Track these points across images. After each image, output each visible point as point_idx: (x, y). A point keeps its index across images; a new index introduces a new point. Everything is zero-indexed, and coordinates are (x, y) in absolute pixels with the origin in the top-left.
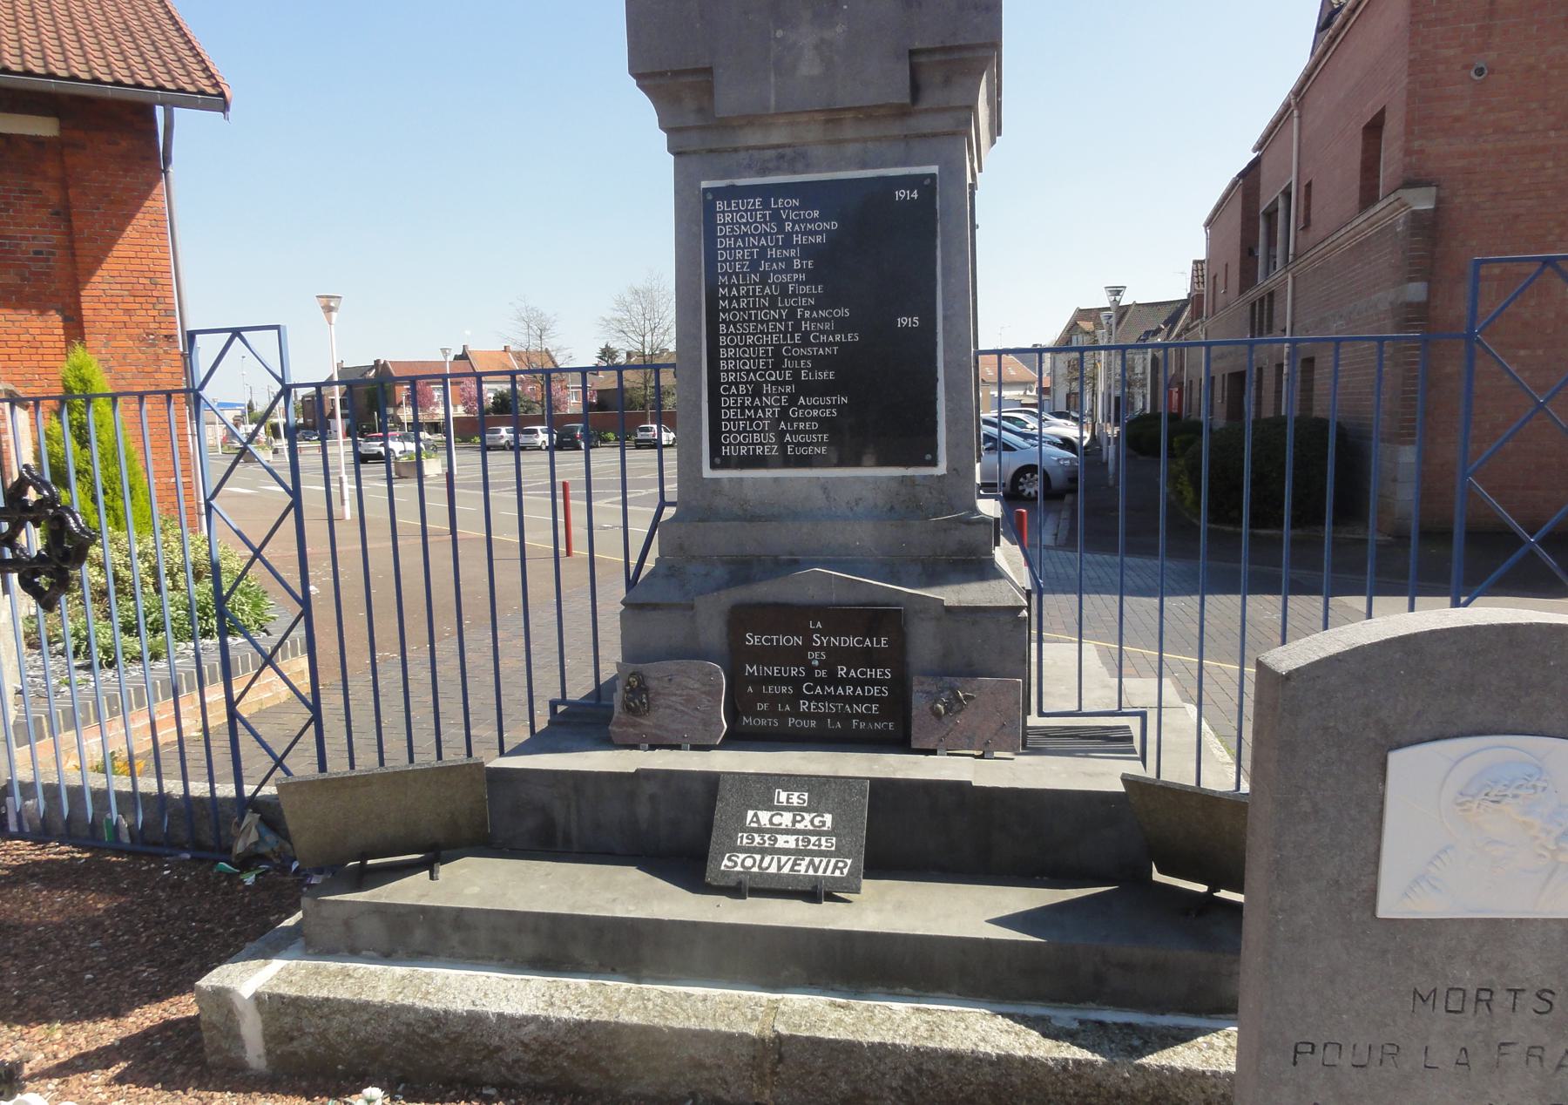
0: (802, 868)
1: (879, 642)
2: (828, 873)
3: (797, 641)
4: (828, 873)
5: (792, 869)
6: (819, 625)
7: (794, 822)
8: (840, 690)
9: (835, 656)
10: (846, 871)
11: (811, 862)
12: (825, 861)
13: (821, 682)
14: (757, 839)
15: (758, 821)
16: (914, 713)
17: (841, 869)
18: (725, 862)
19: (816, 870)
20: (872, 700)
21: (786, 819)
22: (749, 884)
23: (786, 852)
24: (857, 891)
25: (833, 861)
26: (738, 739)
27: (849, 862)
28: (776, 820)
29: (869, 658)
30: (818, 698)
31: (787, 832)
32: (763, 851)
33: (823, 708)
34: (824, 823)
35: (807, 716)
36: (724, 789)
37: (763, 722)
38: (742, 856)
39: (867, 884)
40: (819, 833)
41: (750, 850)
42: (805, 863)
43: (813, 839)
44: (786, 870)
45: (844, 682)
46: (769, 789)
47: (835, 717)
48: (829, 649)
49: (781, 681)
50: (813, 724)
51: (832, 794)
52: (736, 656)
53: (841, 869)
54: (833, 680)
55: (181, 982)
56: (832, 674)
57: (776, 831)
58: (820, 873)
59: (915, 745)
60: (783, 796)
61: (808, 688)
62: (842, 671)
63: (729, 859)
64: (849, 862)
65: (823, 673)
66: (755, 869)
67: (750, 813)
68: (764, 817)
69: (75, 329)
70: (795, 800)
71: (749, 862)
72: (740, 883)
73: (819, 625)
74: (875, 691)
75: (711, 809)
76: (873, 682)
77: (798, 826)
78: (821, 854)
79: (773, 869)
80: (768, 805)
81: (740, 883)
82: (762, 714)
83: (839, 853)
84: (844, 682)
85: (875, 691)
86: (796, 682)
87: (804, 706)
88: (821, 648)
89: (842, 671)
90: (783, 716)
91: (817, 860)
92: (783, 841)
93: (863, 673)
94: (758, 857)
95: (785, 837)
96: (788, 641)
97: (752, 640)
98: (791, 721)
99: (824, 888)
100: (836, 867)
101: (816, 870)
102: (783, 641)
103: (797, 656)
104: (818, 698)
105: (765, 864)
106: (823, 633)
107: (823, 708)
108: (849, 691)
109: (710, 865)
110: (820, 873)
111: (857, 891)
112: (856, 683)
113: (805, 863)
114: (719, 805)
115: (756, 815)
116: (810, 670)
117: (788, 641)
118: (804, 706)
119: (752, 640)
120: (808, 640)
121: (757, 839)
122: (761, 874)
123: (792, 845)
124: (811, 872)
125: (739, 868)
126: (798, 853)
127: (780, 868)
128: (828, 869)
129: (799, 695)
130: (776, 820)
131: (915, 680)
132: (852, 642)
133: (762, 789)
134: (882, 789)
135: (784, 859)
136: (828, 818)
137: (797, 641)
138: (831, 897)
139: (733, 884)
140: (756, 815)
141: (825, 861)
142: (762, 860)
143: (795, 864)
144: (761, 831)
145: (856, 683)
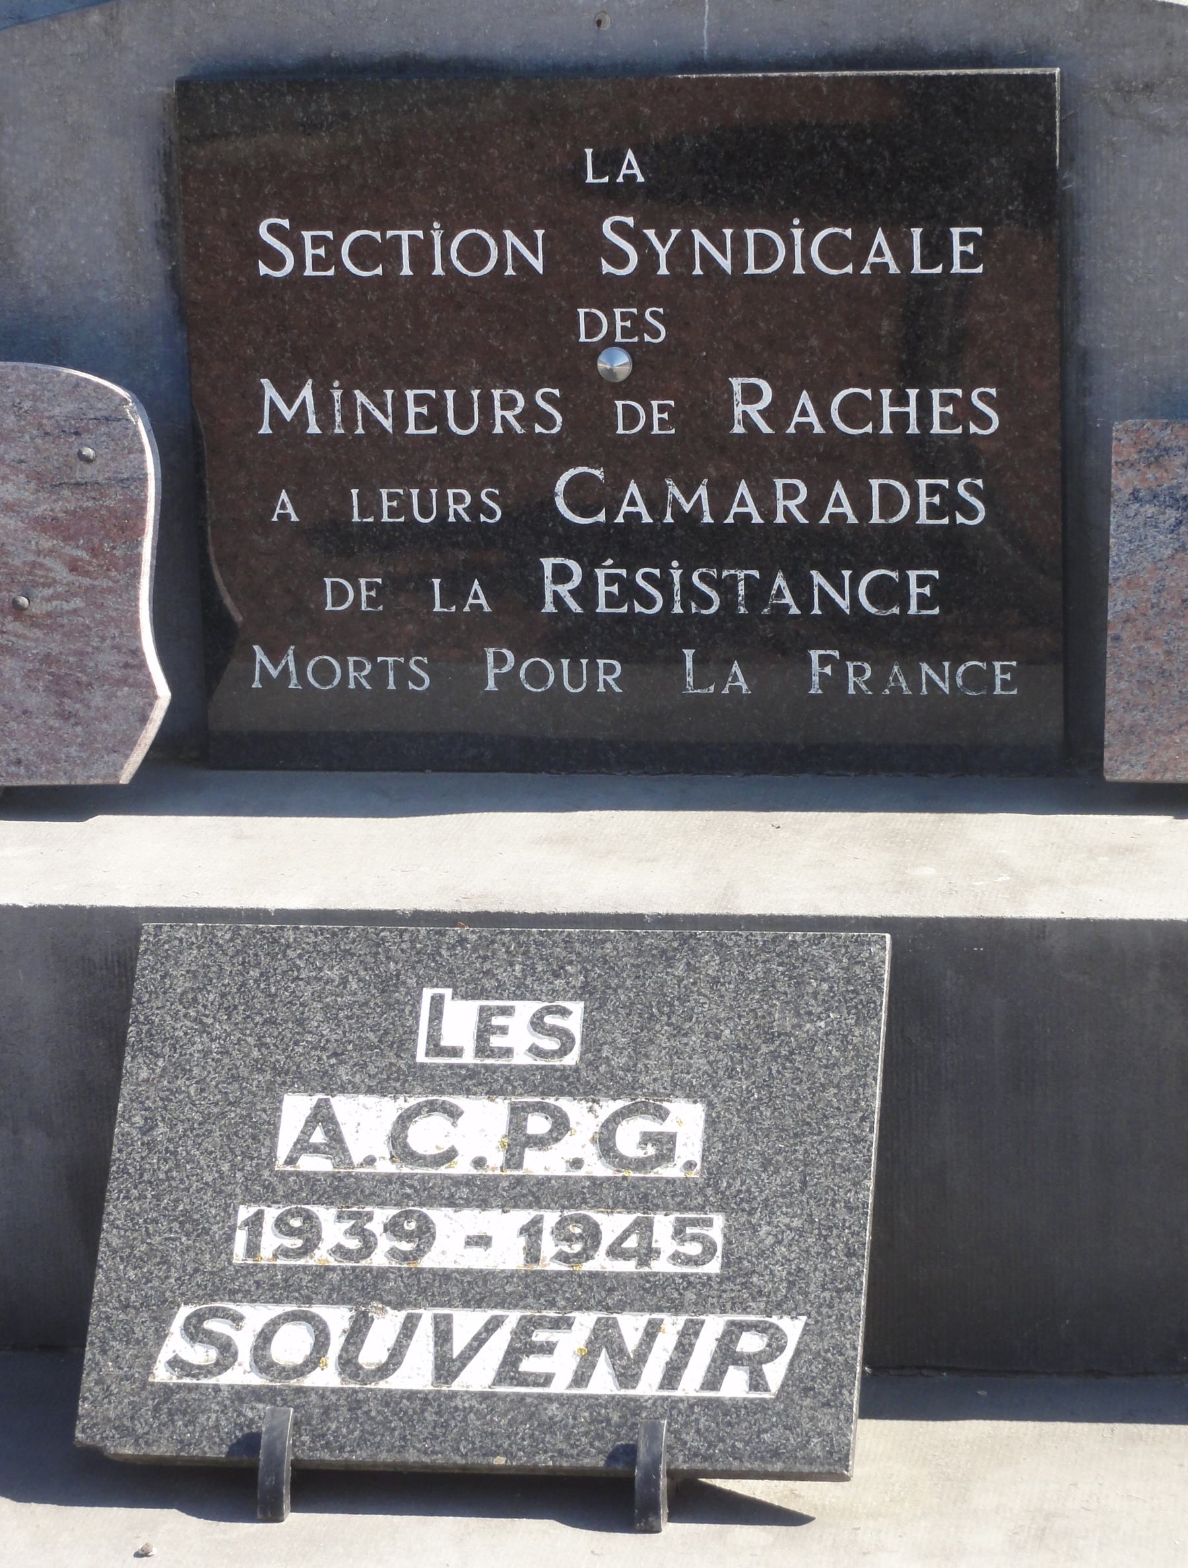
0: (558, 1364)
1: (937, 250)
2: (690, 1385)
3: (521, 251)
4: (690, 1385)
5: (509, 1369)
6: (631, 166)
7: (518, 1142)
8: (634, 502)
9: (714, 328)
10: (775, 1373)
11: (605, 1339)
12: (672, 1325)
13: (650, 461)
14: (333, 1229)
15: (336, 1144)
16: (1118, 602)
17: (754, 1364)
18: (176, 1344)
19: (628, 1374)
20: (902, 545)
21: (475, 1132)
22: (295, 1447)
23: (476, 1288)
24: (834, 1467)
25: (714, 1325)
26: (217, 756)
27: (792, 1328)
28: (427, 1135)
29: (919, 335)
30: (629, 544)
31: (479, 1192)
32: (362, 1288)
33: (659, 591)
34: (665, 1146)
35: (576, 636)
36: (159, 998)
37: (355, 673)
38: (257, 1315)
39: (878, 1442)
40: (640, 1195)
41: (294, 1287)
42: (570, 1343)
43: (612, 1224)
44: (478, 1376)
45: (758, 459)
46: (387, 984)
47: (722, 637)
48: (684, 294)
49: (443, 460)
50: (609, 675)
51: (706, 1007)
52: (207, 346)
53: (754, 1364)
54: (706, 447)
55: (383, 227)
56: (703, 420)
57: (425, 1189)
58: (649, 1384)
59: (1122, 766)
60: (460, 1021)
61: (580, 495)
62: (749, 406)
63: (195, 1331)
64: (792, 1328)
65: (655, 416)
66: (326, 1377)
67: (295, 1109)
68: (366, 1122)
69: (454, 1124)
70: (519, 1037)
71: (292, 1344)
72: (250, 1442)
73: (631, 166)
74: (918, 500)
75: (98, 1098)
76: (916, 455)
77: (536, 1163)
78: (654, 1294)
79: (416, 1373)
80: (388, 1063)
81: (250, 1442)
82: (349, 635)
83: (738, 1286)
84: (758, 459)
85: (918, 500)
86: (514, 463)
87: (559, 585)
88: (643, 287)
89: (749, 406)
90: (457, 642)
91: (631, 1326)
92: (457, 1239)
93: (854, 411)
94: (337, 1318)
95: (473, 1220)
96: (474, 252)
97: (290, 251)
98: (497, 665)
99: (669, 1455)
100: (726, 1355)
101: (628, 1374)
102: (447, 254)
103: (522, 329)
104: (629, 544)
105: (373, 1353)
106: (657, 202)
107: (659, 591)
108: (790, 505)
109: (100, 1366)
110: (649, 1384)
111: (834, 1467)
112: (823, 460)
113: (570, 1343)
114: (137, 1069)
115: (322, 1116)
116: (587, 394)
117: (474, 252)
118: (559, 585)
119: (290, 251)
120: (577, 248)
121: (333, 1229)
122: (354, 1402)
123: (506, 1255)
124: (603, 1382)
125: (242, 1374)
126: (539, 1294)
127: (446, 1367)
128: (681, 1365)
129: (533, 528)
130: (427, 1135)
131: (1124, 439)
132: (802, 249)
133: (355, 986)
134: (949, 979)
135: (467, 1323)
136: (687, 1121)
137: (521, 251)
138: (698, 1501)
139: (215, 1451)
140: (322, 1116)
141: (672, 1325)
142: (357, 1332)
143: (521, 1347)
144: (349, 1191)
145: (823, 460)
